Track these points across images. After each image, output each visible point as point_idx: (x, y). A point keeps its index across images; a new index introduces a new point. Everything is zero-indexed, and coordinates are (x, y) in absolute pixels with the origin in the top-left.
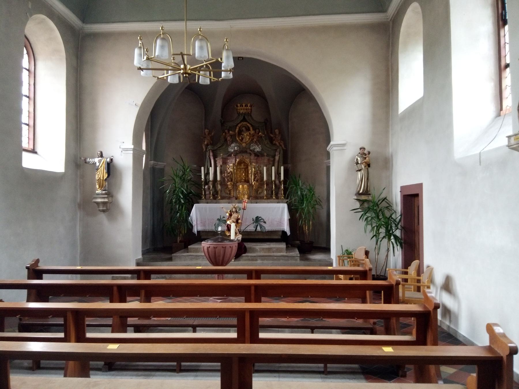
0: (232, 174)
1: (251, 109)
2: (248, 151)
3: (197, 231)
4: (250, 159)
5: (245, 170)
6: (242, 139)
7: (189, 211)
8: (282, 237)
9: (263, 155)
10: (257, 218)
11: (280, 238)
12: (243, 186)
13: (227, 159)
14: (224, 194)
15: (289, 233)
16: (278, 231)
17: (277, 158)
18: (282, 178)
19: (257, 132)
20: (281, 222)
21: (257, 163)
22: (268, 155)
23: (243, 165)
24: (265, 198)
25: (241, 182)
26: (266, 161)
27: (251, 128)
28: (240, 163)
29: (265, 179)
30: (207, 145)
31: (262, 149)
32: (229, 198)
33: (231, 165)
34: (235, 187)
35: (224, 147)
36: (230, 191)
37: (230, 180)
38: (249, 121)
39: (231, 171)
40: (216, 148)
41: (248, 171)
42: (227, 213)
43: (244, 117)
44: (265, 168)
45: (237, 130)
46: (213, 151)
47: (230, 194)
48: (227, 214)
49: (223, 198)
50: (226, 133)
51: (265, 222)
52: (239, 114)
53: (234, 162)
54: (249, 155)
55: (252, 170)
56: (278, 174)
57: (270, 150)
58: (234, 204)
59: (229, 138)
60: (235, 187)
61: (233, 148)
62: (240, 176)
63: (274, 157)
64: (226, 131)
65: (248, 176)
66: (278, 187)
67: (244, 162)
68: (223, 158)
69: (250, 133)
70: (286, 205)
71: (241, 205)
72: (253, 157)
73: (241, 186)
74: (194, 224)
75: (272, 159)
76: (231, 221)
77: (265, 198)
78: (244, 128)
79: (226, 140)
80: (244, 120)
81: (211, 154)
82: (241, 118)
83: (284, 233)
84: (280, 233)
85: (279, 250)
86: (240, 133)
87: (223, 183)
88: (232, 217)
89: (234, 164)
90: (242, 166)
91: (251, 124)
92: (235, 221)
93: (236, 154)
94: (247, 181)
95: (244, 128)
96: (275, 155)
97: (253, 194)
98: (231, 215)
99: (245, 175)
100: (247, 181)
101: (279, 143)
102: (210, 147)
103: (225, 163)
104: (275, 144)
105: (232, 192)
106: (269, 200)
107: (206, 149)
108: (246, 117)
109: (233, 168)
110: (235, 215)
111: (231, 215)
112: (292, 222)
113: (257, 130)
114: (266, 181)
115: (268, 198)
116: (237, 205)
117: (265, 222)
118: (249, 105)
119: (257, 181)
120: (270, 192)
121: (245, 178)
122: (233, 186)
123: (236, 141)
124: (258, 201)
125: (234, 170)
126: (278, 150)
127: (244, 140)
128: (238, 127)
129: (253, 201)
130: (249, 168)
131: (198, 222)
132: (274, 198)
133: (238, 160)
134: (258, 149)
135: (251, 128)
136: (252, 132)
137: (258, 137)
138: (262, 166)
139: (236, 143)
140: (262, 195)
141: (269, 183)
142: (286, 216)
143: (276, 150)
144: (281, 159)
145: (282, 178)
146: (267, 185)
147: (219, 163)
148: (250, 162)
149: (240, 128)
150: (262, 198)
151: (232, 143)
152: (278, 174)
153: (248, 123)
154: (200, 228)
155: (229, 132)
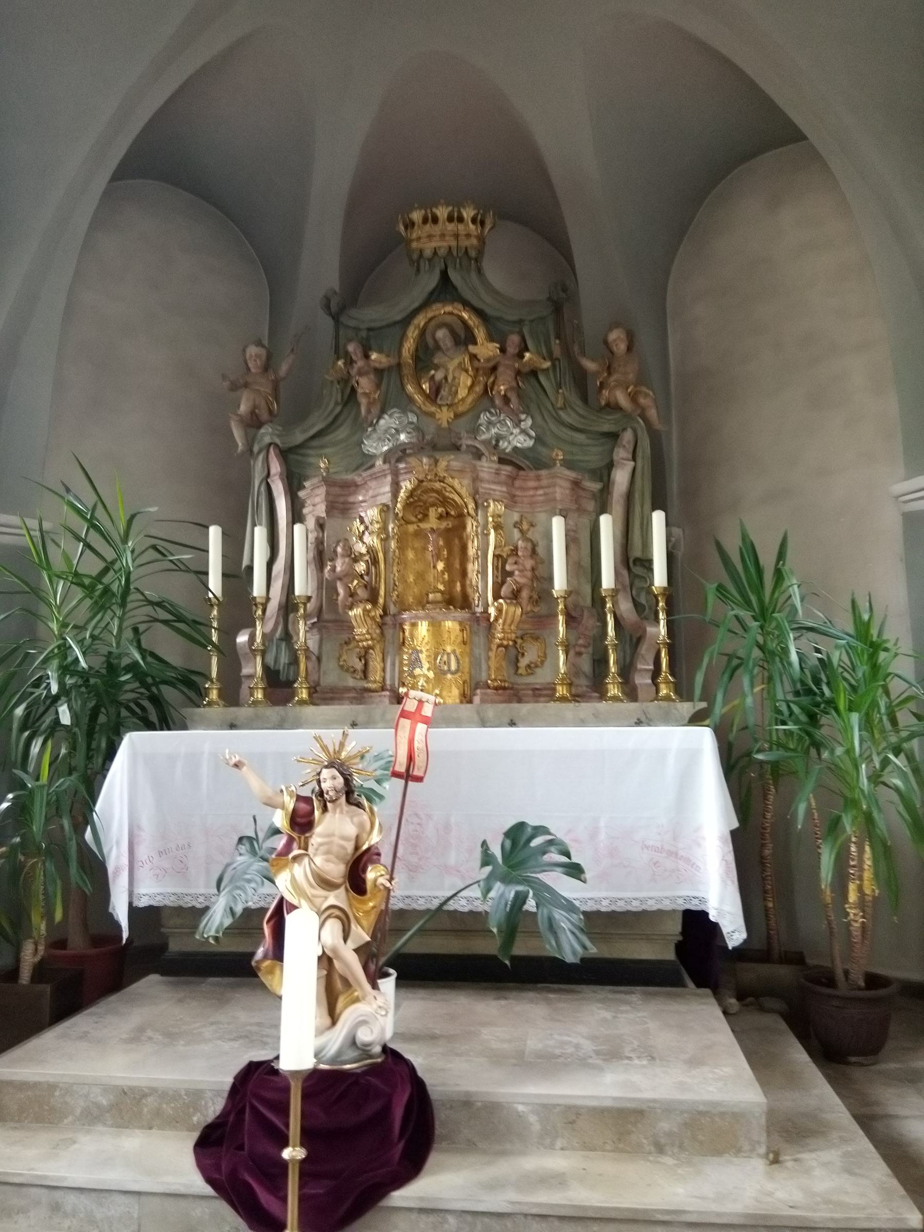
0: (375, 561)
1: (481, 239)
2: (466, 442)
3: (134, 912)
4: (476, 479)
5: (449, 545)
6: (437, 389)
7: (91, 784)
8: (692, 955)
9: (547, 465)
10: (518, 835)
11: (670, 955)
12: (435, 626)
13: (352, 487)
14: (331, 677)
15: (734, 931)
16: (660, 913)
17: (621, 478)
18: (660, 578)
19: (512, 350)
20: (675, 855)
21: (511, 501)
22: (569, 464)
23: (434, 516)
24: (561, 691)
25: (423, 603)
26: (561, 490)
27: (480, 334)
28: (417, 504)
29: (560, 583)
30: (253, 423)
31: (538, 440)
32: (361, 696)
33: (372, 514)
34: (389, 632)
35: (342, 433)
36: (364, 656)
37: (362, 593)
38: (468, 295)
39: (371, 551)
40: (299, 437)
41: (464, 549)
42: (272, 805)
43: (444, 275)
44: (558, 525)
45: (409, 346)
46: (285, 454)
47: (365, 672)
48: (280, 819)
49: (321, 695)
50: (350, 362)
51: (575, 871)
52: (417, 262)
53: (386, 499)
54: (468, 457)
55: (484, 544)
56: (634, 563)
57: (581, 438)
58: (332, 736)
59: (365, 384)
60: (389, 626)
61: (388, 432)
62: (421, 576)
63: (604, 473)
64: (351, 348)
65: (464, 573)
66: (631, 640)
67: (445, 501)
68: (328, 482)
69: (473, 357)
70: (704, 740)
71: (374, 742)
72: (487, 466)
73: (423, 629)
74: (116, 859)
75: (596, 486)
76: (300, 871)
77: (561, 691)
78: (441, 334)
79: (351, 397)
80: (446, 290)
81: (276, 467)
82: (431, 281)
83: (697, 924)
84: (675, 927)
85: (705, 1134)
86: (425, 357)
87: (329, 619)
88: (316, 838)
89: (385, 510)
90: (433, 522)
91: (479, 313)
92: (337, 870)
93: (399, 454)
94: (458, 600)
95: (441, 334)
96: (610, 466)
97: (493, 668)
98: (302, 823)
99: (448, 568)
100: (458, 600)
101: (633, 398)
102: (267, 434)
103: (340, 506)
104: (613, 407)
105: (376, 663)
106: (586, 708)
107: (250, 443)
108: (453, 275)
109: (384, 528)
110: (336, 827)
111: (302, 823)
112: (757, 852)
113: (513, 340)
114: (569, 593)
115: (577, 697)
116: (358, 740)
117: (575, 871)
118: (468, 213)
119: (515, 596)
120: (586, 664)
121: (450, 584)
122: (381, 626)
123: (405, 404)
124: (524, 708)
125: (385, 541)
126: (628, 436)
127: (444, 392)
128: (412, 333)
129: (491, 711)
130: (471, 526)
131: (143, 853)
132: (613, 690)
133: (406, 485)
134: (518, 439)
135: (480, 334)
136: (486, 349)
137: (518, 373)
138: (541, 517)
139: (404, 411)
140: (542, 677)
141: (588, 605)
142: (712, 814)
143: (614, 437)
144: (645, 486)
145: (660, 578)
146: (571, 620)
147: (316, 503)
148: (475, 495)
149: (423, 333)
150: (545, 693)
151: (383, 411)
152: (634, 563)
153: (466, 304)
154: (152, 891)
155: (367, 357)
